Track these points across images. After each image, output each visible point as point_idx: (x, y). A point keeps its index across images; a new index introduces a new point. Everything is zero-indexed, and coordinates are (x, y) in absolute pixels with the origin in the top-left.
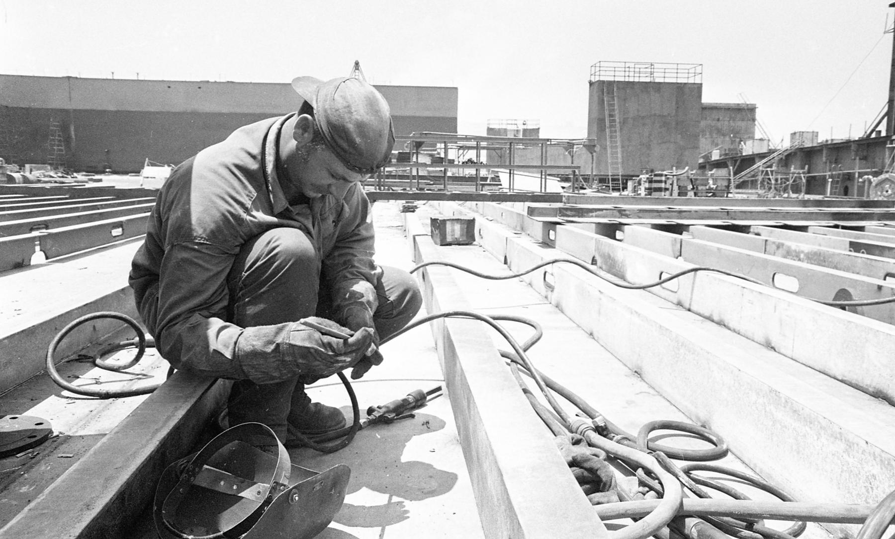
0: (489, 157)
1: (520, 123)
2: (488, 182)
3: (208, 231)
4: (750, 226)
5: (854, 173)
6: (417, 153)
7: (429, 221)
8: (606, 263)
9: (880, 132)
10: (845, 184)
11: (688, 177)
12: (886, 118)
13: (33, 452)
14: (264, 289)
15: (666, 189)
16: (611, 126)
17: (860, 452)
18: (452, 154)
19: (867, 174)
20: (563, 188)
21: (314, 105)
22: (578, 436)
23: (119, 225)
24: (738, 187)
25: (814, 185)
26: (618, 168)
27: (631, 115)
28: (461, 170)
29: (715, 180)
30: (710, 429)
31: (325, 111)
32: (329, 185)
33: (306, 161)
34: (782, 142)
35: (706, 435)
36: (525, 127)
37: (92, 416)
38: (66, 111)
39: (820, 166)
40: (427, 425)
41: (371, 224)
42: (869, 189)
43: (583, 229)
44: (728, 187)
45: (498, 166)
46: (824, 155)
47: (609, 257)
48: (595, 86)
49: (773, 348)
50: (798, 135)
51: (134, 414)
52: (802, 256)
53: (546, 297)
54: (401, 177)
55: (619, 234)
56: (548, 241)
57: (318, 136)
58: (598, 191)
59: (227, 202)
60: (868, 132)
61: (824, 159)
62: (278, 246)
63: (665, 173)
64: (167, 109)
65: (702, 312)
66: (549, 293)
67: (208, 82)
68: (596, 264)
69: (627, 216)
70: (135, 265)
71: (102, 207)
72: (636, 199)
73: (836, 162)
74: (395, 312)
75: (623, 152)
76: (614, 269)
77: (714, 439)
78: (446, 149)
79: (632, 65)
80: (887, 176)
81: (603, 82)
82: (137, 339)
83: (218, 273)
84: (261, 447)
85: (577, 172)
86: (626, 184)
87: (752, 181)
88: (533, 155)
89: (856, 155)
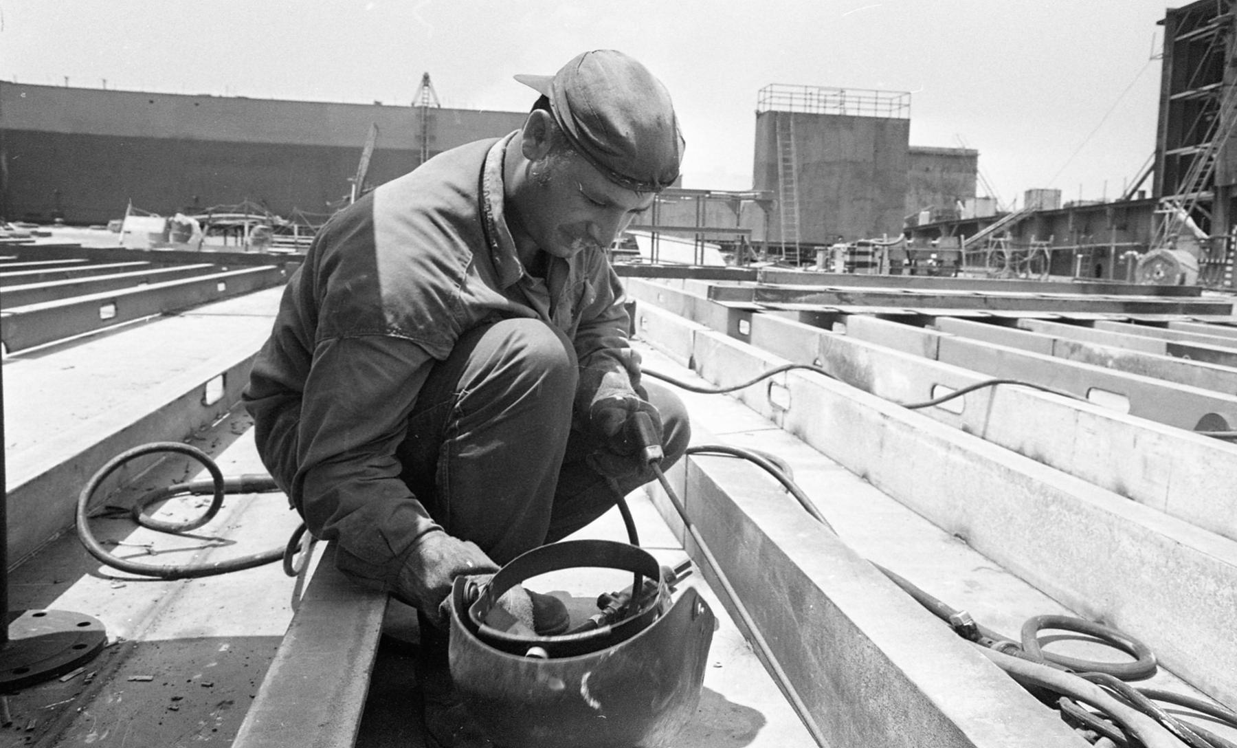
4: (934, 317)
5: (1109, 248)
9: (1143, 193)
10: (1098, 263)
12: (1152, 174)
13: (85, 672)
14: (499, 417)
15: (874, 265)
16: (785, 175)
19: (1127, 248)
23: (112, 301)
25: (1060, 263)
26: (794, 235)
27: (814, 159)
34: (1012, 202)
35: (1115, 637)
43: (788, 317)
47: (844, 361)
48: (765, 120)
50: (1034, 195)
53: (773, 420)
55: (836, 325)
58: (775, 265)
60: (1128, 193)
61: (1070, 227)
62: (522, 349)
63: (872, 241)
64: (149, 133)
67: (209, 96)
69: (849, 302)
73: (1087, 232)
75: (801, 210)
77: (1130, 645)
79: (815, 91)
81: (776, 113)
85: (746, 239)
89: (1113, 222)
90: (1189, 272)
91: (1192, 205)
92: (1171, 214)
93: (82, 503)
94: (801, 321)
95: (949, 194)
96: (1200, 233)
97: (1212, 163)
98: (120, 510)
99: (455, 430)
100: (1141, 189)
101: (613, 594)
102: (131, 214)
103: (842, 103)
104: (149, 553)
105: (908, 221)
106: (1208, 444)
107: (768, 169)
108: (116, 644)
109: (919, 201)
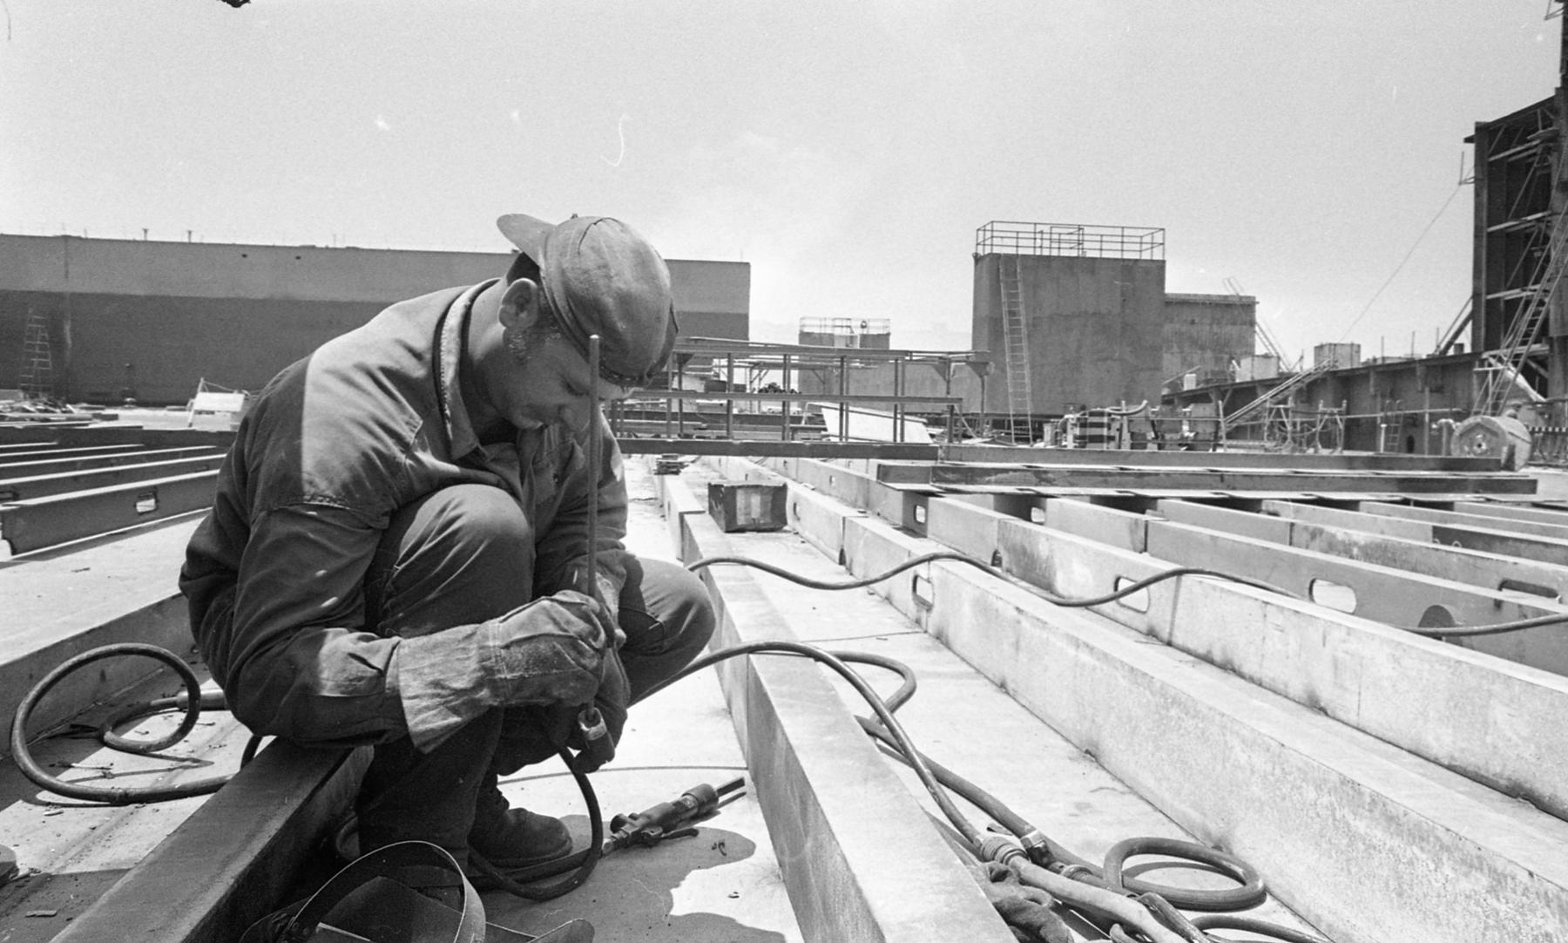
0: (802, 381)
1: (856, 324)
2: (803, 424)
3: (337, 486)
4: (1156, 499)
5: (1423, 416)
6: (680, 375)
7: (706, 491)
8: (1018, 564)
9: (1461, 346)
11: (1147, 418)
15: (1111, 438)
16: (1012, 331)
17: (1520, 890)
18: (740, 376)
19: (1445, 415)
20: (932, 436)
21: (541, 262)
22: (998, 866)
24: (1230, 436)
25: (1358, 434)
26: (1023, 404)
28: (756, 403)
29: (1193, 424)
30: (1231, 853)
31: (563, 272)
32: (561, 408)
33: (521, 362)
34: (1298, 358)
36: (865, 332)
37: (95, 836)
38: (60, 296)
39: (1366, 403)
40: (726, 849)
41: (623, 480)
42: (1449, 442)
44: (1217, 437)
45: (821, 398)
46: (1372, 382)
47: (1025, 552)
48: (985, 264)
49: (1323, 711)
51: (182, 830)
52: (1355, 551)
54: (650, 415)
55: (1036, 514)
56: (912, 525)
57: (547, 318)
59: (371, 433)
60: (1443, 346)
61: (1372, 390)
63: (1108, 410)
65: (1191, 646)
66: (924, 614)
67: (313, 247)
68: (999, 565)
69: (1050, 483)
70: (192, 553)
71: (119, 462)
72: (1062, 454)
73: (1393, 395)
74: (666, 644)
76: (1035, 575)
77: (1240, 871)
78: (730, 367)
79: (1046, 229)
80: (1478, 419)
81: (999, 256)
82: (185, 694)
83: (354, 563)
84: (420, 891)
85: (957, 410)
86: (1041, 429)
87: (1253, 427)
88: (880, 379)
89: (1426, 384)
90: (1519, 443)
91: (1522, 360)
92: (1496, 373)
93: (20, 715)
94: (996, 509)
95: (1221, 352)
96: (1535, 396)
97: (1543, 309)
98: (86, 729)
99: (386, 611)
100: (1458, 341)
101: (631, 816)
102: (204, 390)
103: (1080, 243)
104: (105, 776)
105: (1170, 385)
106: (1397, 639)
107: (992, 321)
108: (27, 876)
109: (1184, 359)
